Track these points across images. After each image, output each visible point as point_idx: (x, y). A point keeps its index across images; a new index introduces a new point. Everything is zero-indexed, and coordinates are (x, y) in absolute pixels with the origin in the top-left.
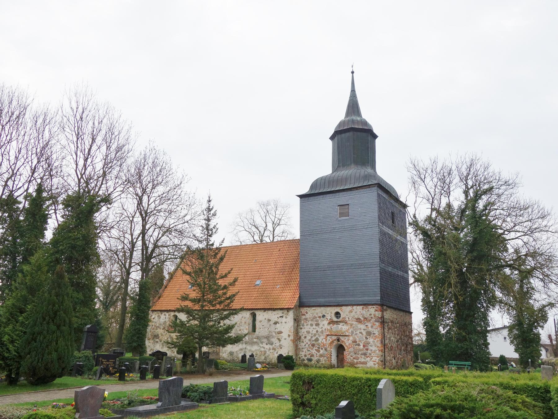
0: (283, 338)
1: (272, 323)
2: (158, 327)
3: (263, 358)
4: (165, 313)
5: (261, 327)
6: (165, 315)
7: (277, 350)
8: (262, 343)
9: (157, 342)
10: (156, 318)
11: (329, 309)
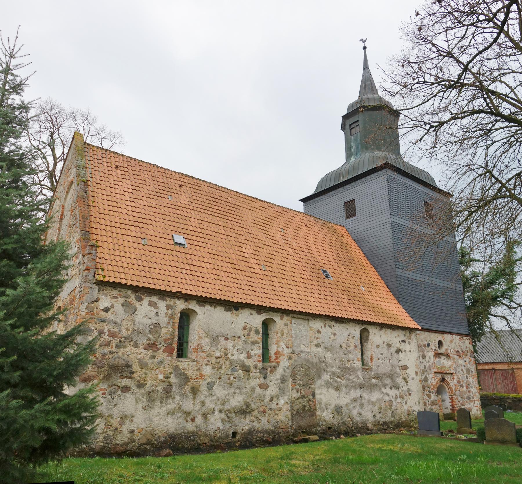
0: (410, 378)
1: (393, 350)
2: (128, 339)
3: (390, 414)
4: (155, 299)
5: (380, 356)
6: (152, 304)
7: (405, 397)
8: (385, 386)
9: (126, 389)
10: (118, 308)
11: (433, 335)
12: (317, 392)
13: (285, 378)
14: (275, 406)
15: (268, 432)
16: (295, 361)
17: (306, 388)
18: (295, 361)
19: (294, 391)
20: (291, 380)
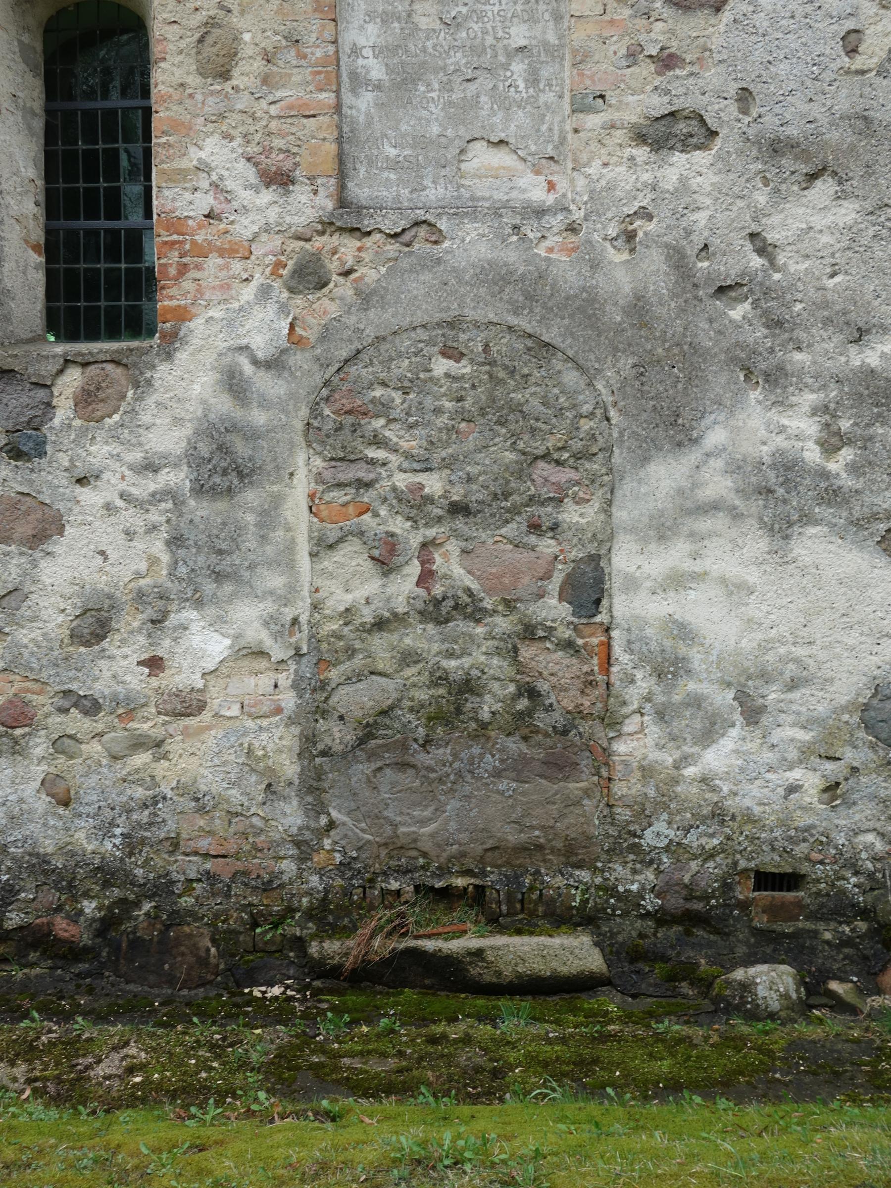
12: (624, 560)
13: (241, 449)
14: (137, 680)
15: (64, 879)
16: (366, 298)
17: (497, 541)
18: (366, 298)
19: (352, 558)
20: (304, 468)
